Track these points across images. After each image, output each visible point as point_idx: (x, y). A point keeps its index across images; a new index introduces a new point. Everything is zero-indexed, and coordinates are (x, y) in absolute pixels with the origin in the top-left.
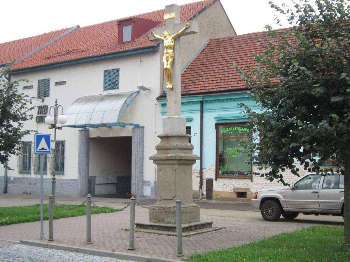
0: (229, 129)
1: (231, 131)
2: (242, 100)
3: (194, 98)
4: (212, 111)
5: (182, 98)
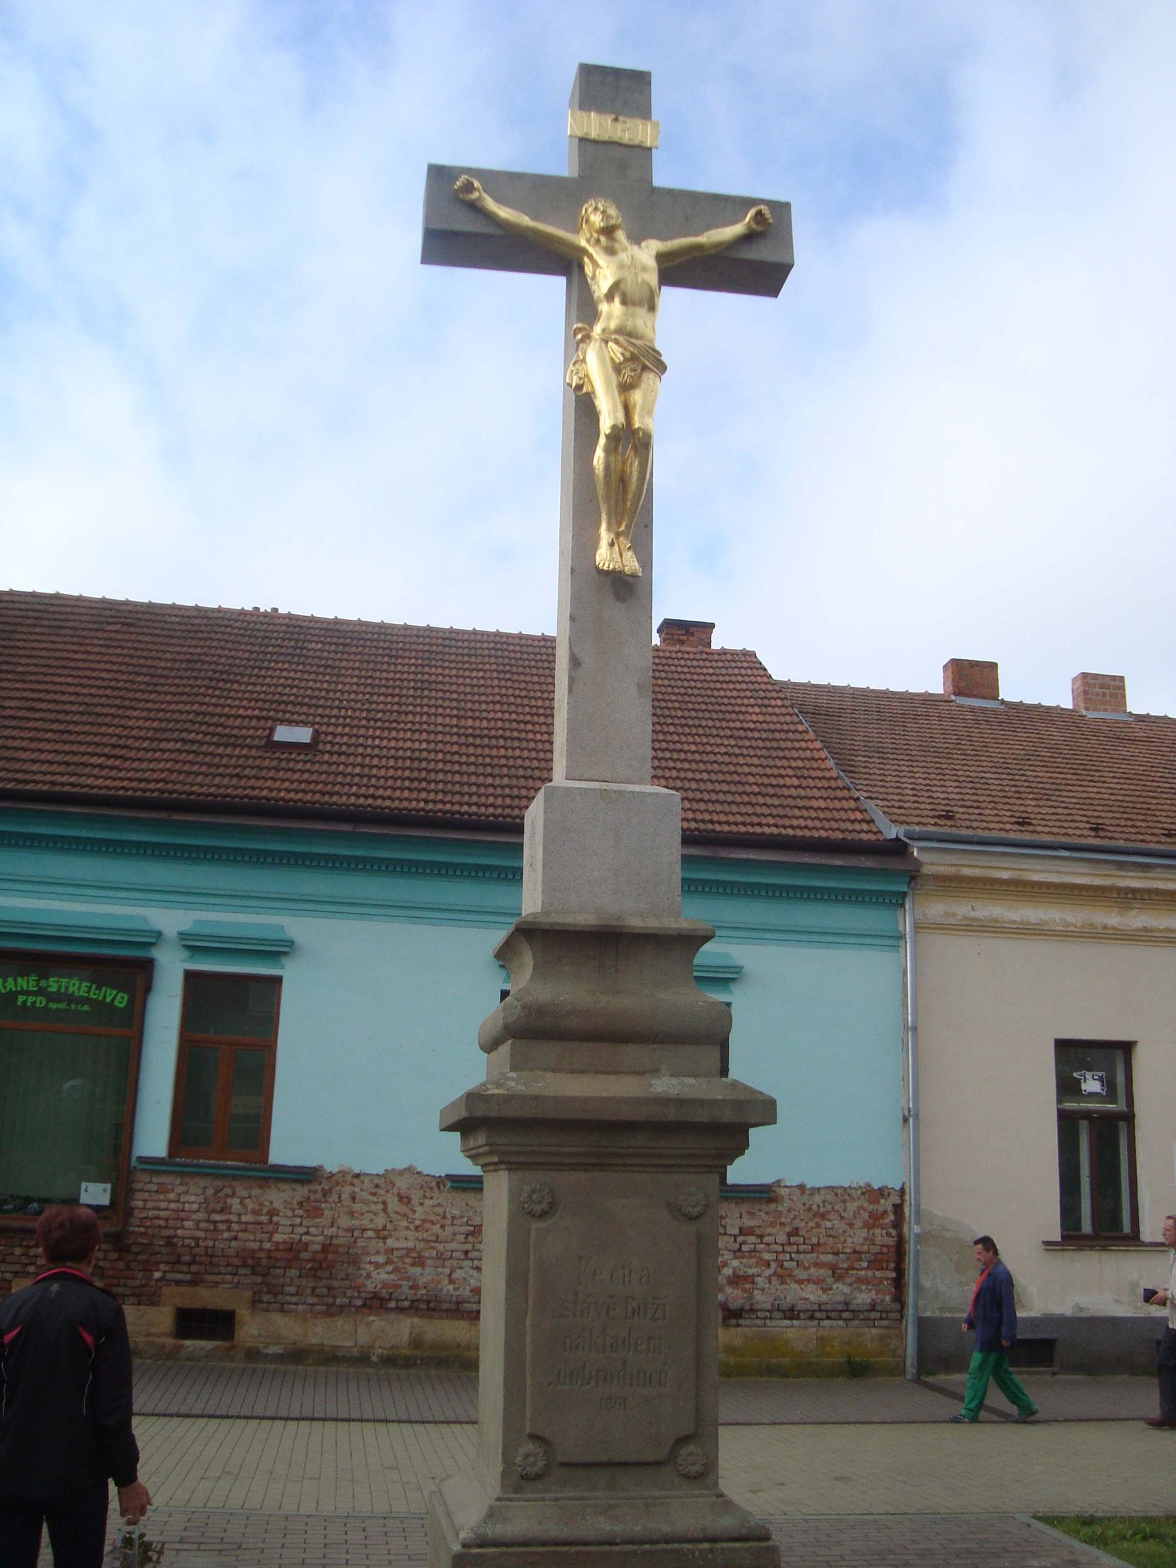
0: (16, 981)
1: (28, 993)
2: (100, 849)
3: (289, 834)
4: (456, 916)
5: (686, 859)
